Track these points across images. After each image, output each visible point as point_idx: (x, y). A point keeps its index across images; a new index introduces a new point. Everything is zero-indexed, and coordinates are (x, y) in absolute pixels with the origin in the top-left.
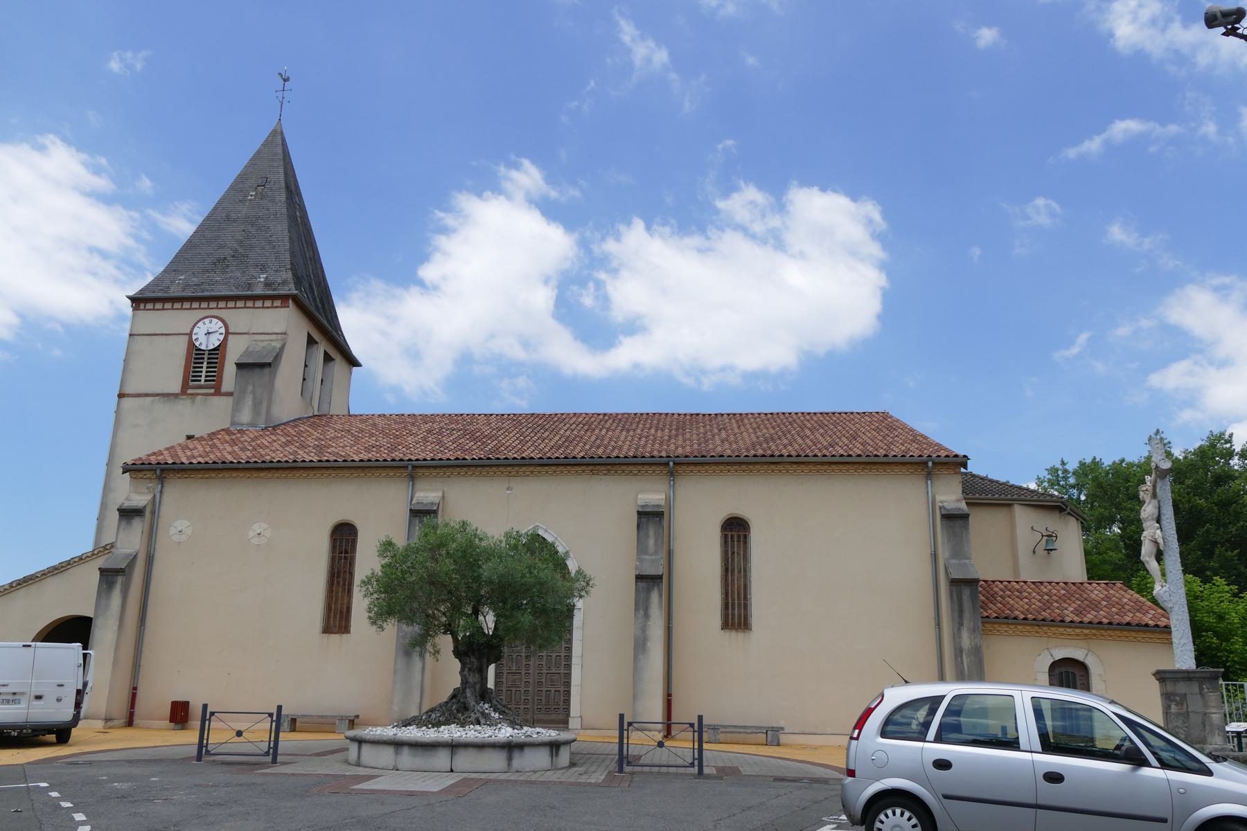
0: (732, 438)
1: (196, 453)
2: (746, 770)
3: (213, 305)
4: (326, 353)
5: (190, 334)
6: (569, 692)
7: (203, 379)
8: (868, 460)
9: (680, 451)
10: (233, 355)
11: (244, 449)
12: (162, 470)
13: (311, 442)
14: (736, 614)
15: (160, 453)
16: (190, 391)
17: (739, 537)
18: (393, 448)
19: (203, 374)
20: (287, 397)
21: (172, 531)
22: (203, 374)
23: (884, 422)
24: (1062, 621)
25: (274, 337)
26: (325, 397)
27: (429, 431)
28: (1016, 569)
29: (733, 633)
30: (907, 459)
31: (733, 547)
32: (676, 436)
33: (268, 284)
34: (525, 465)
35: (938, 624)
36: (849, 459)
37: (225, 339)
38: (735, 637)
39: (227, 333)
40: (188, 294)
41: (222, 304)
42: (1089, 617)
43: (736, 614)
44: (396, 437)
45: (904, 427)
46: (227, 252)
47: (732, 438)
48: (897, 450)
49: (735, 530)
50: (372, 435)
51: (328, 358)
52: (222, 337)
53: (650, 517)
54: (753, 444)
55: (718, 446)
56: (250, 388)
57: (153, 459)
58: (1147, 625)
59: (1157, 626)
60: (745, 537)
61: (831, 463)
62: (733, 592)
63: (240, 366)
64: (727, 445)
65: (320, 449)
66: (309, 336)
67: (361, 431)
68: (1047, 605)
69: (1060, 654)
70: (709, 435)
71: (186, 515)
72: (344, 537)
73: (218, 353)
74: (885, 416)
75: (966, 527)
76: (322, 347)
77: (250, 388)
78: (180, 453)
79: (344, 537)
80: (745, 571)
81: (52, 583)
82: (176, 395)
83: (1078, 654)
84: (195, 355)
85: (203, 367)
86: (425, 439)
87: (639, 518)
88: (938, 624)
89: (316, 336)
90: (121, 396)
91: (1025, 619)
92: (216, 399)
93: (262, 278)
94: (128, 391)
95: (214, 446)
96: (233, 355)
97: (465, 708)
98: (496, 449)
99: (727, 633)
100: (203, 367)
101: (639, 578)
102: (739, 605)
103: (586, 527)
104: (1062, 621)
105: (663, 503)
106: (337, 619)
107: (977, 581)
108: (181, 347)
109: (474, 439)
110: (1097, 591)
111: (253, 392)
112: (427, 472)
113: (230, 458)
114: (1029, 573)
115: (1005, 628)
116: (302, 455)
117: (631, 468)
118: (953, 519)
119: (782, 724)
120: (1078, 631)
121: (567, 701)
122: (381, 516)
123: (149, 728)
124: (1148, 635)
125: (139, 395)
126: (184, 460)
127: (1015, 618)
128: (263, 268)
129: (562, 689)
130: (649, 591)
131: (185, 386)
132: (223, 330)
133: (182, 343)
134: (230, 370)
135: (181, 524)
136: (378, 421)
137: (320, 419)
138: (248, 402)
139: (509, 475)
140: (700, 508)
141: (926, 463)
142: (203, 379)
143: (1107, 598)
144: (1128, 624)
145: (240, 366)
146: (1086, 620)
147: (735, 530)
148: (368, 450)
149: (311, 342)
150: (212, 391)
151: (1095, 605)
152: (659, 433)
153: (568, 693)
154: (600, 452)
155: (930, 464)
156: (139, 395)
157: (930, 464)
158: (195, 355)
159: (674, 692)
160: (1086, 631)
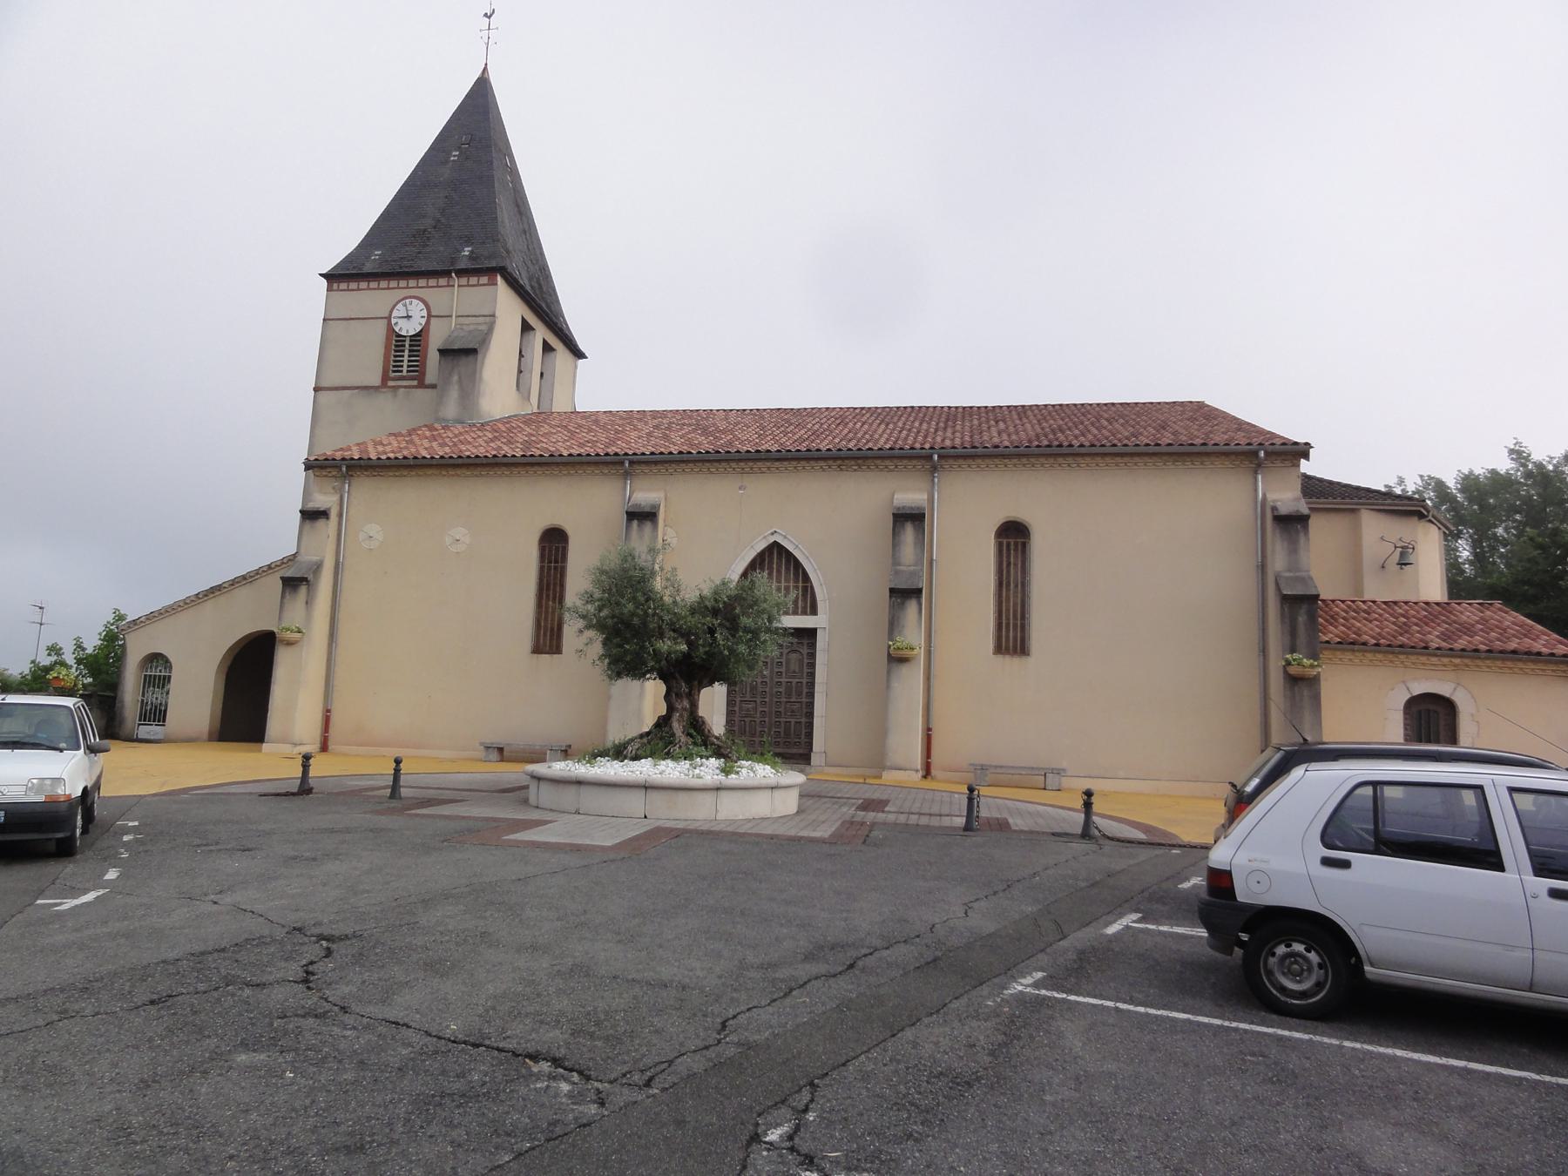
0: (1011, 429)
1: (388, 449)
2: (1016, 823)
3: (412, 283)
4: (545, 342)
5: (389, 318)
6: (811, 724)
7: (405, 369)
8: (1182, 449)
9: (948, 443)
10: (436, 341)
11: (443, 445)
12: (348, 467)
13: (521, 438)
14: (1012, 636)
15: (349, 449)
16: (391, 383)
17: (1016, 544)
18: (612, 442)
19: (405, 364)
20: (498, 390)
21: (361, 536)
22: (405, 364)
23: (1200, 412)
24: (1426, 648)
25: (481, 319)
26: (546, 392)
27: (656, 427)
28: (1358, 585)
29: (1008, 658)
30: (1232, 447)
31: (1008, 556)
32: (945, 429)
33: (472, 257)
34: (760, 460)
35: (1264, 651)
36: (1157, 449)
37: (428, 323)
38: (1011, 663)
39: (430, 316)
40: (386, 269)
41: (422, 282)
42: (1461, 643)
43: (1012, 636)
44: (617, 432)
45: (1225, 416)
46: (429, 222)
47: (1011, 429)
48: (1219, 438)
49: (1013, 535)
50: (590, 430)
51: (547, 348)
52: (423, 321)
53: (910, 519)
54: (1037, 436)
55: (992, 436)
56: (455, 378)
57: (338, 456)
58: (1539, 654)
59: (1552, 655)
60: (1024, 545)
61: (1132, 455)
62: (1008, 610)
63: (443, 352)
64: (1005, 436)
65: (527, 445)
66: (524, 322)
67: (580, 426)
68: (1405, 629)
69: (1419, 688)
70: (984, 426)
71: (375, 514)
72: (554, 542)
73: (419, 339)
74: (1201, 406)
75: (1306, 528)
76: (541, 333)
77: (455, 378)
78: (371, 449)
79: (554, 542)
80: (1024, 585)
81: (242, 593)
82: (376, 388)
83: (1443, 688)
84: (396, 342)
85: (406, 358)
86: (649, 434)
87: (895, 522)
88: (1264, 651)
89: (533, 320)
90: (316, 389)
91: (1377, 645)
92: (420, 391)
93: (467, 251)
94: (324, 384)
95: (411, 442)
96: (436, 341)
97: (670, 740)
98: (730, 443)
99: (1000, 658)
100: (406, 358)
101: (892, 591)
102: (1015, 626)
103: (830, 526)
104: (1426, 648)
105: (925, 505)
106: (547, 639)
107: (1316, 597)
108: (378, 333)
109: (705, 432)
110: (1468, 611)
111: (460, 381)
112: (645, 468)
113: (425, 453)
114: (1376, 590)
115: (1349, 655)
116: (507, 450)
117: (887, 462)
118: (1291, 524)
119: (1064, 765)
120: (1446, 660)
121: (810, 735)
122: (589, 513)
123: (345, 755)
124: (1541, 666)
125: (337, 389)
126: (373, 457)
127: (1364, 644)
128: (468, 241)
129: (803, 720)
130: (902, 606)
131: (385, 378)
132: (425, 313)
133: (380, 329)
134: (433, 357)
135: (373, 529)
136: (601, 417)
137: (541, 417)
138: (454, 394)
139: (743, 472)
140: (966, 513)
141: (1256, 453)
142: (405, 369)
143: (1484, 621)
144: (1514, 652)
145: (443, 352)
146: (1457, 646)
147: (1013, 535)
148: (581, 445)
149: (526, 327)
150: (415, 383)
151: (1468, 630)
152: (925, 426)
153: (810, 725)
154: (851, 445)
155: (1262, 454)
156: (337, 389)
157: (1262, 454)
158: (396, 342)
159: (933, 725)
160: (1457, 661)
